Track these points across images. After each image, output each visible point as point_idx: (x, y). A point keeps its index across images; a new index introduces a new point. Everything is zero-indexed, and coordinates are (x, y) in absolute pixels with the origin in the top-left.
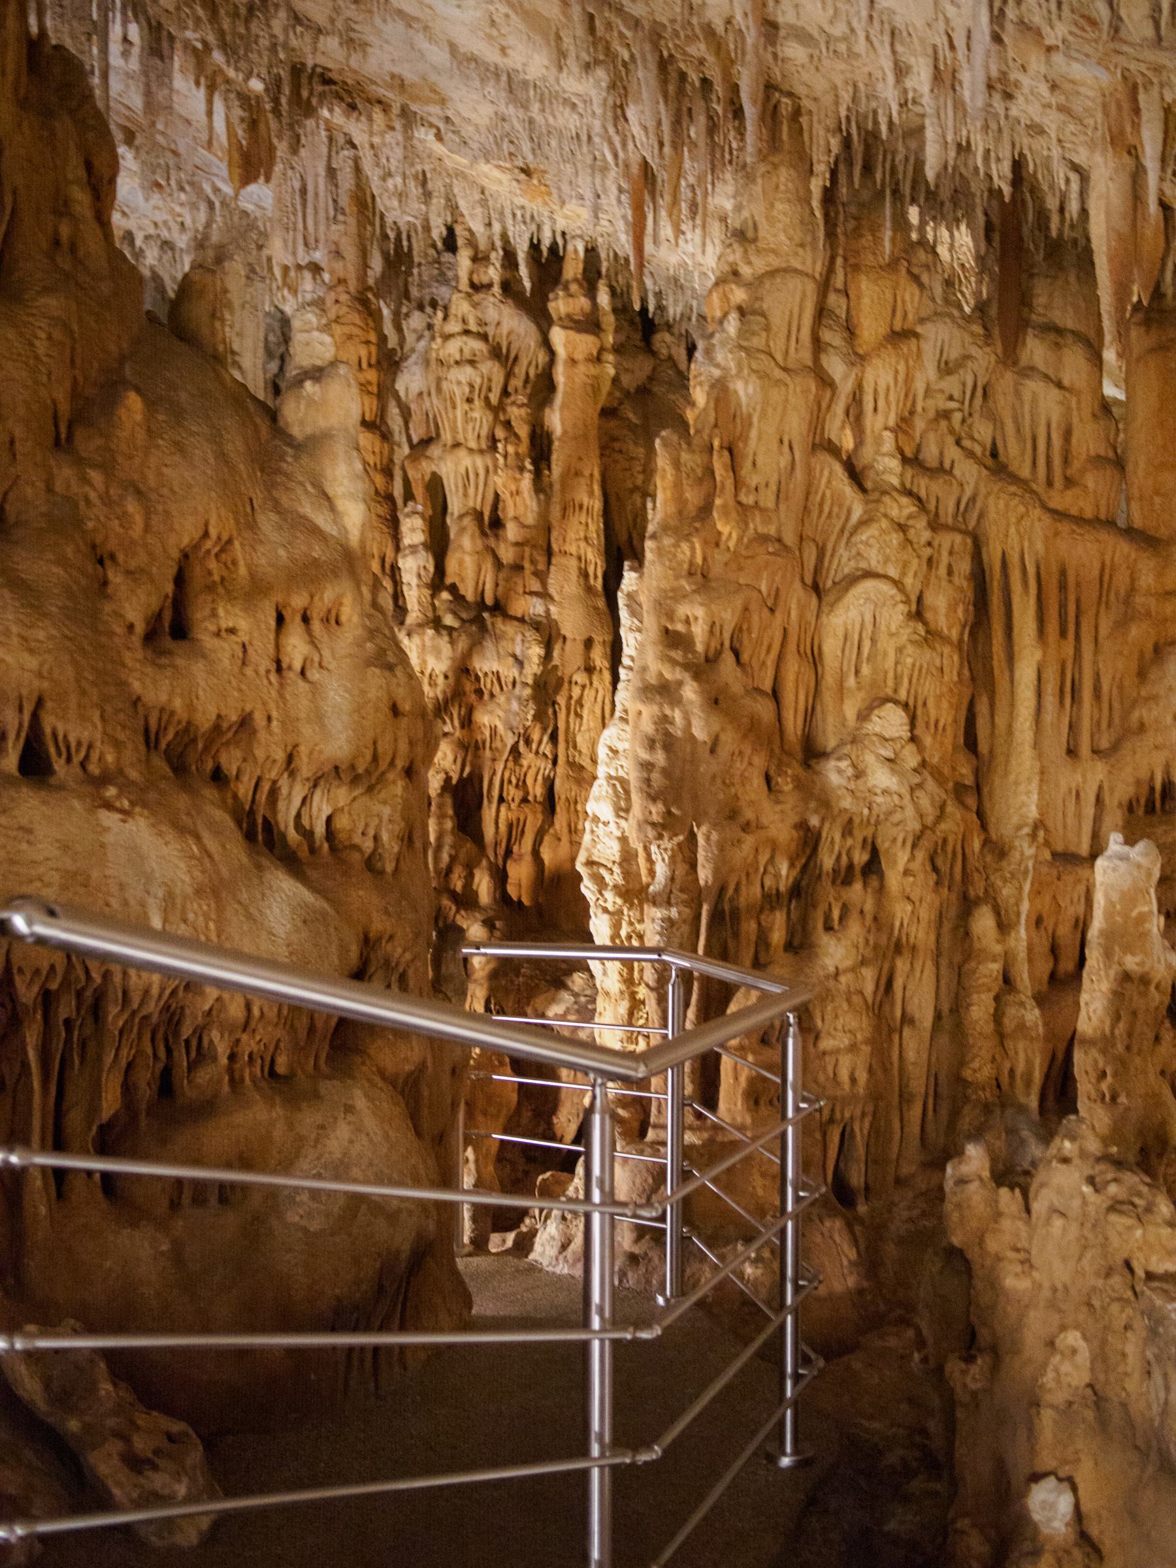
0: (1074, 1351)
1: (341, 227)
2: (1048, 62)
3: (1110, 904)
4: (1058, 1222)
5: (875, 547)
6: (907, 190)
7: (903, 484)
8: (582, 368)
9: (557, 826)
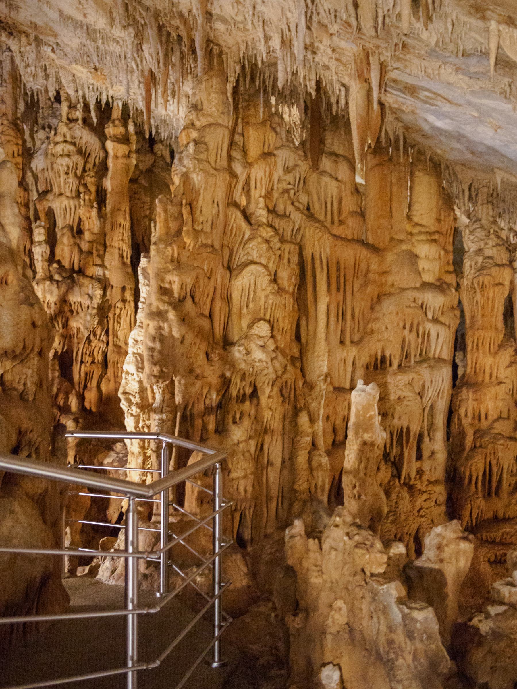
0: (340, 609)
1: (5, 89)
2: (331, 39)
3: (358, 411)
4: (334, 553)
5: (255, 250)
6: (270, 89)
7: (268, 222)
8: (121, 161)
9: (109, 374)
